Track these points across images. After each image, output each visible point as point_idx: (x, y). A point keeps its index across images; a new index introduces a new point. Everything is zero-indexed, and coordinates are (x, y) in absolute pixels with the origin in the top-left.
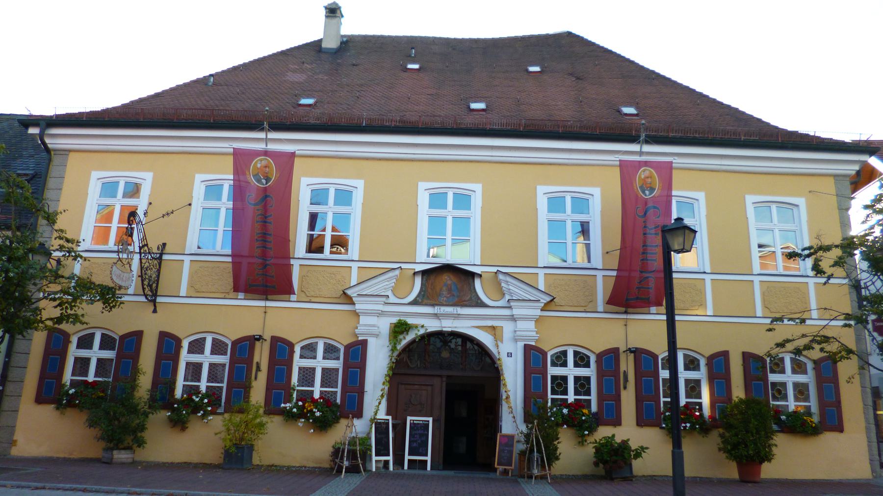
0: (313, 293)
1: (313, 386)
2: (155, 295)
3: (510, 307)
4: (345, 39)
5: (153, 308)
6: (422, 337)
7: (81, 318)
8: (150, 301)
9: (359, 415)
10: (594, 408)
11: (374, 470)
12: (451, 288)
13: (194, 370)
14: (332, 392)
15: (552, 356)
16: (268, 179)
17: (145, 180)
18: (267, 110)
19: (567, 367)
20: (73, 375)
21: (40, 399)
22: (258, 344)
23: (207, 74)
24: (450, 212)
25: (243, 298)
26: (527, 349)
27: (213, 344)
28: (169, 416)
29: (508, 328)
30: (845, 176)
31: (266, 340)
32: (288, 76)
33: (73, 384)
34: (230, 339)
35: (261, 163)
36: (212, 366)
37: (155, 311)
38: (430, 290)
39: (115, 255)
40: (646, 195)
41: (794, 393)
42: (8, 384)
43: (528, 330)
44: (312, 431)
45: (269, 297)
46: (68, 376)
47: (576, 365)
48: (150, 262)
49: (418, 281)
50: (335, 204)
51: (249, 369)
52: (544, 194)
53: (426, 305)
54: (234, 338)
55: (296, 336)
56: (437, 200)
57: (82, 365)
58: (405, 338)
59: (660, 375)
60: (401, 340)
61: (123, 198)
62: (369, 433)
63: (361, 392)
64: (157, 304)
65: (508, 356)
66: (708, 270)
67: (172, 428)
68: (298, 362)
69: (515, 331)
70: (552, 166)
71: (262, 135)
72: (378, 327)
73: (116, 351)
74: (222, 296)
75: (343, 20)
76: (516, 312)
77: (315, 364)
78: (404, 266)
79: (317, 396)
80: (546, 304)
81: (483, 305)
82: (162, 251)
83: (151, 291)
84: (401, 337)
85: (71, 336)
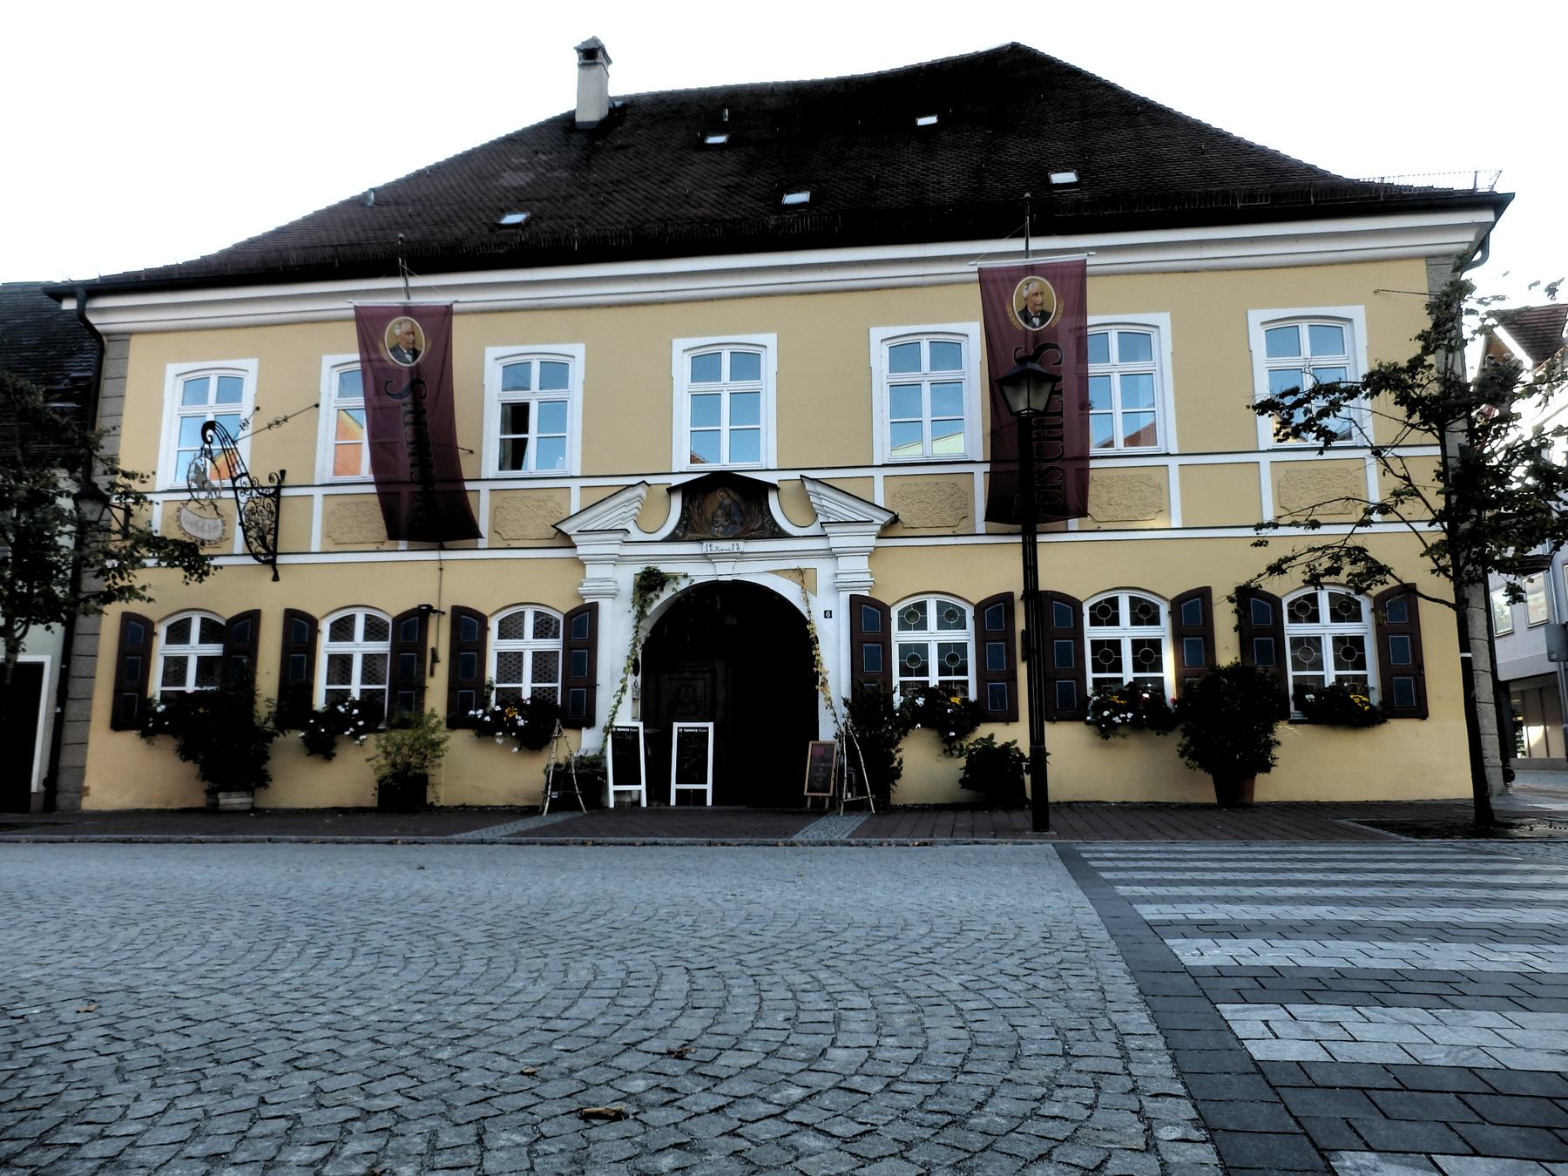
0: (511, 534)
1: (520, 680)
2: (274, 553)
3: (825, 536)
4: (618, 104)
5: (271, 574)
6: (687, 593)
7: (140, 591)
8: (265, 563)
9: (590, 723)
10: (972, 695)
11: (612, 805)
12: (730, 511)
13: (340, 666)
14: (549, 688)
15: (1092, 608)
16: (415, 354)
17: (573, 357)
18: (401, 239)
19: (926, 629)
20: (164, 684)
21: (119, 722)
22: (433, 620)
23: (366, 189)
24: (726, 386)
25: (405, 548)
26: (856, 603)
27: (366, 624)
28: (302, 737)
29: (824, 570)
30: (1448, 255)
31: (444, 613)
32: (502, 177)
33: (165, 697)
34: (389, 615)
35: (400, 328)
36: (537, 656)
37: (276, 578)
38: (696, 517)
39: (187, 496)
40: (1034, 326)
41: (1335, 656)
42: (69, 703)
43: (857, 571)
44: (516, 749)
45: (446, 544)
46: (156, 687)
47: (1135, 621)
48: (257, 501)
49: (677, 503)
50: (1122, 359)
51: (422, 660)
52: (684, 351)
53: (690, 541)
54: (396, 612)
55: (488, 601)
56: (705, 366)
57: (176, 668)
58: (658, 597)
59: (1286, 632)
60: (652, 600)
61: (541, 389)
62: (603, 750)
63: (592, 686)
64: (278, 568)
65: (826, 617)
66: (1174, 450)
67: (309, 755)
68: (495, 645)
69: (836, 574)
70: (716, 304)
71: (398, 283)
72: (616, 582)
73: (389, 642)
74: (373, 547)
75: (610, 69)
76: (835, 542)
77: (1121, 635)
78: (649, 480)
79: (526, 694)
80: (885, 527)
81: (783, 535)
82: (279, 482)
83: (265, 546)
84: (652, 595)
85: (156, 625)
